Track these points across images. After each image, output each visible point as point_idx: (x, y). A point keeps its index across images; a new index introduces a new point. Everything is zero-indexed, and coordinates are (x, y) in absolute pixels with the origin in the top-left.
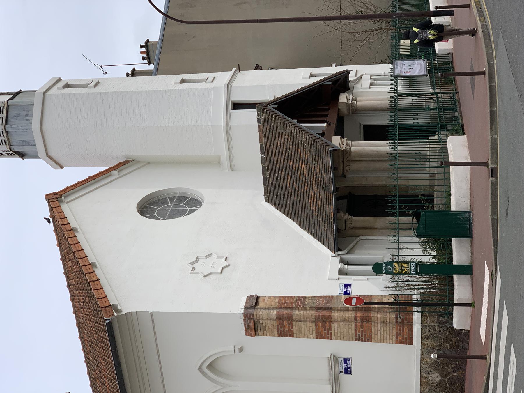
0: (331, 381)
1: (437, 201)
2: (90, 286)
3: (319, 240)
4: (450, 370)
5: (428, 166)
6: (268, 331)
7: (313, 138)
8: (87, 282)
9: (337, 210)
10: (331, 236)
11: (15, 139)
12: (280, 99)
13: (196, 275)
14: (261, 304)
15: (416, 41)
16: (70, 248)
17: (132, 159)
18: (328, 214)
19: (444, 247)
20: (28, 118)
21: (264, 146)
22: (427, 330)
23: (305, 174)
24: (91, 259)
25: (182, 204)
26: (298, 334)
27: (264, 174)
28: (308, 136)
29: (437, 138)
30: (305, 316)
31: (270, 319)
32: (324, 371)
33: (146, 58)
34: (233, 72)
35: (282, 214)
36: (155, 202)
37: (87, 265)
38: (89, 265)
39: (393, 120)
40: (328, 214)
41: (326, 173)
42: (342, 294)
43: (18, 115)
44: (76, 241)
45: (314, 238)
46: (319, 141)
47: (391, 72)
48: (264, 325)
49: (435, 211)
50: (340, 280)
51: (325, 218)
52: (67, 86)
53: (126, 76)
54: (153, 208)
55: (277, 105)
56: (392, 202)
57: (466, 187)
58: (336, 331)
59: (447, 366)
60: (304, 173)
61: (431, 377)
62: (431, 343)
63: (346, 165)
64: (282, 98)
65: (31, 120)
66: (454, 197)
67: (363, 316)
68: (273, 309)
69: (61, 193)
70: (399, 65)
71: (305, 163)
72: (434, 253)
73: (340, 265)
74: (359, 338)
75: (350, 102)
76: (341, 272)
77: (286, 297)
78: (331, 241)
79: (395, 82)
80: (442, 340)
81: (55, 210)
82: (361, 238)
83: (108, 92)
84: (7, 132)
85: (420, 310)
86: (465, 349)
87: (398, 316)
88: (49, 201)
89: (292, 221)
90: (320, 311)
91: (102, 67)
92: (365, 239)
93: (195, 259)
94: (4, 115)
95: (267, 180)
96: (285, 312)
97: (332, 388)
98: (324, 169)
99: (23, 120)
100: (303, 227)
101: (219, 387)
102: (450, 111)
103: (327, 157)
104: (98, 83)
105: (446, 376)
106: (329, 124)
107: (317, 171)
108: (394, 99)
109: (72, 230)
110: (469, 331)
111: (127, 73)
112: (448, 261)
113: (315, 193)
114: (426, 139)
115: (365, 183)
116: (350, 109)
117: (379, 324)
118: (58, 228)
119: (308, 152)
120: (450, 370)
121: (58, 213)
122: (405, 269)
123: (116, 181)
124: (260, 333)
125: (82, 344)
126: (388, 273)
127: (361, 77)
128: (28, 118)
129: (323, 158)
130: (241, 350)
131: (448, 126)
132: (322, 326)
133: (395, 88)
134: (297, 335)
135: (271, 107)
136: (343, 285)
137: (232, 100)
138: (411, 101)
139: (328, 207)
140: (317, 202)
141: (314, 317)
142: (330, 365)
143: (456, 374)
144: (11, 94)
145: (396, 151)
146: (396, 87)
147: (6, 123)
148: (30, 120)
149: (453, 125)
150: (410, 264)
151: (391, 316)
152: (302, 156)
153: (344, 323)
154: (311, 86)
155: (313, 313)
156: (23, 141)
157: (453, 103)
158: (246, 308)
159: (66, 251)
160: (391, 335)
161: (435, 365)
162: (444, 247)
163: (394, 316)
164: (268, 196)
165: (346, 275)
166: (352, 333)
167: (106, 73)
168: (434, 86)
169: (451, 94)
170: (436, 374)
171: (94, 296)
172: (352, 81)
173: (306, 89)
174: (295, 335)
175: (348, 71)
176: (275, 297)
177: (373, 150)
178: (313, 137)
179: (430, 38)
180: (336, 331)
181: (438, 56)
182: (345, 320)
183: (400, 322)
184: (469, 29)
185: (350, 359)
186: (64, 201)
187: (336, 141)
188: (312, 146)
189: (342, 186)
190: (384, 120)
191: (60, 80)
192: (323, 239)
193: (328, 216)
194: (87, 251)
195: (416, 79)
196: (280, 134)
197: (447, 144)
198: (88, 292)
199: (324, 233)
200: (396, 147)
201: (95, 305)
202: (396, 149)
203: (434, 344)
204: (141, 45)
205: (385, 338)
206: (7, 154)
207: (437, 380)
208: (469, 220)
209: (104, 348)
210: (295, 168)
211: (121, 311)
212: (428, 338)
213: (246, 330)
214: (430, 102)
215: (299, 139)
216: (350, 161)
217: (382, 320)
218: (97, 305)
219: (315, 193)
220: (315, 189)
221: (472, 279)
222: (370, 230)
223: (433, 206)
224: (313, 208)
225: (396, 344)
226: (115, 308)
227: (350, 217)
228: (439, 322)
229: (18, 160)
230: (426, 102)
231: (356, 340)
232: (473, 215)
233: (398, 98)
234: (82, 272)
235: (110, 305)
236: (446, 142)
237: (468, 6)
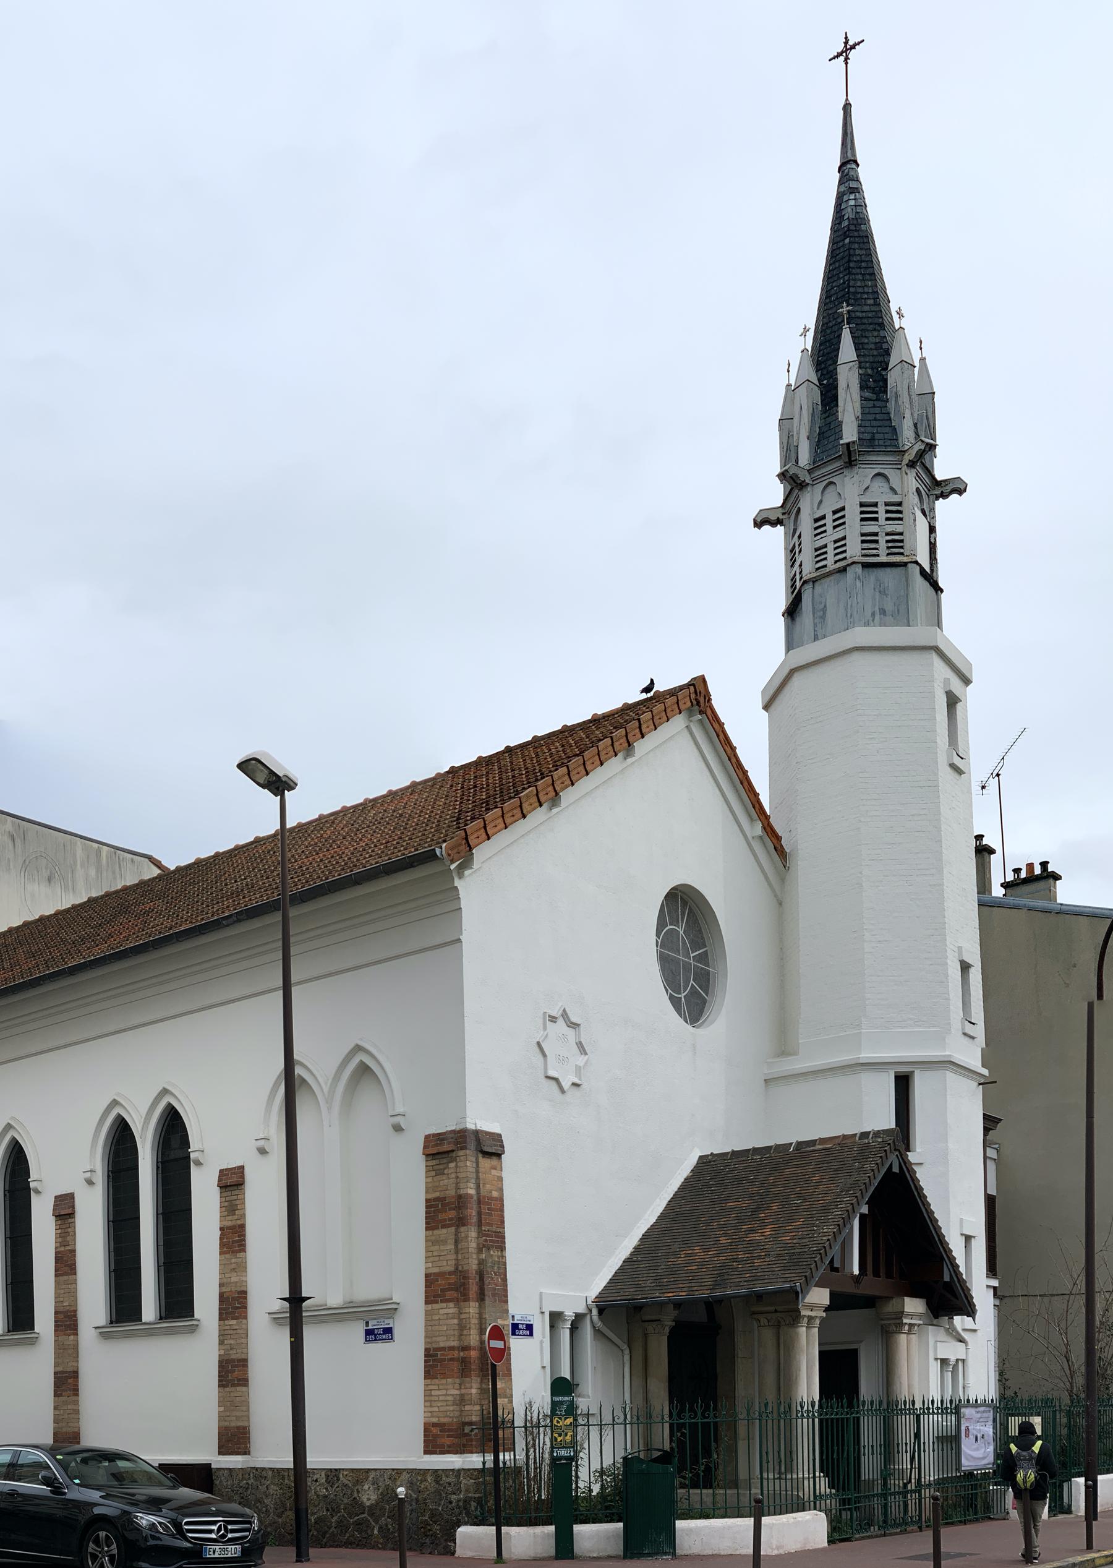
0: (350, 1304)
1: (695, 1494)
2: (511, 798)
3: (620, 1271)
4: (383, 1521)
5: (765, 1475)
6: (435, 1179)
7: (824, 1250)
8: (517, 791)
9: (678, 1305)
10: (627, 1294)
11: (829, 591)
12: (911, 1177)
13: (542, 1026)
14: (485, 1163)
15: (1013, 1448)
16: (591, 745)
17: (788, 865)
18: (669, 1287)
19: (607, 1508)
20: (877, 617)
21: (812, 1148)
22: (452, 1479)
23: (751, 1237)
24: (568, 796)
25: (692, 982)
26: (433, 1238)
27: (755, 1151)
28: (828, 1240)
29: (823, 1492)
30: (466, 1251)
31: (457, 1183)
32: (367, 1291)
33: (1018, 876)
34: (979, 1071)
35: (674, 1193)
36: (696, 922)
37: (554, 788)
38: (555, 791)
39: (872, 1407)
40: (669, 1287)
41: (751, 1279)
42: (513, 1320)
43: (883, 593)
44: (607, 756)
45: (623, 1260)
46: (815, 1262)
47: (968, 1401)
48: (446, 1172)
49: (673, 1490)
50: (540, 1315)
51: (662, 1281)
52: (952, 701)
53: (976, 834)
54: (682, 921)
55: (898, 1171)
56: (692, 1410)
57: (724, 1547)
58: (442, 1312)
59: (388, 1517)
60: (754, 1235)
61: (369, 1488)
62: (429, 1487)
63: (769, 1318)
64: (913, 1180)
65: (872, 624)
66: (702, 1525)
67: (472, 1361)
68: (478, 1188)
69: (709, 712)
70: (985, 1415)
71: (774, 1236)
72: (596, 1489)
73: (570, 1314)
74: (431, 1356)
75: (905, 1321)
76: (555, 1318)
77: (502, 1210)
78: (616, 1295)
79: (947, 1408)
80: (434, 1507)
81: (671, 701)
82: (627, 1352)
83: (939, 797)
84: (843, 570)
85: (487, 1466)
86: (421, 1548)
87: (474, 1427)
88: (691, 685)
89: (659, 1214)
90: (477, 1280)
91: (997, 778)
92: (625, 1360)
93: (574, 1019)
94: (883, 559)
95: (742, 1159)
96: (472, 1212)
97: (337, 1306)
98: (759, 1274)
99: (874, 606)
100: (646, 1237)
101: (326, 1090)
102: (880, 1516)
103: (783, 1280)
104: (959, 771)
105: (372, 1515)
106: (857, 1280)
107: (756, 1261)
108: (910, 1408)
109: (629, 745)
110: (453, 1553)
111: (983, 836)
112: (581, 1515)
113: (713, 1259)
114: (821, 1471)
115: (740, 1356)
116: (889, 1322)
117: (457, 1392)
118: (631, 713)
119: (795, 1241)
120: (384, 1522)
121: (665, 711)
122: (561, 1438)
123: (739, 831)
124: (430, 1163)
125: (401, 790)
126: (554, 1405)
127: (961, 1340)
128: (877, 617)
129: (782, 1272)
130: (398, 1128)
131: (849, 1513)
132: (449, 1284)
133: (933, 1409)
134: (429, 1238)
135: (893, 1158)
136: (530, 1321)
137: (916, 1073)
138: (904, 1441)
139: (684, 1285)
140: (694, 1264)
141: (465, 1269)
142: (379, 1302)
143: (376, 1532)
144: (932, 571)
145: (797, 1416)
146: (936, 1411)
147: (865, 566)
148: (873, 621)
149: (852, 1522)
150: (572, 1447)
151: (474, 1413)
152: (787, 1228)
153: (457, 1327)
154: (940, 1240)
155: (473, 1265)
156: (824, 610)
157: (898, 1521)
158: (477, 1133)
159: (584, 736)
160: (440, 1414)
161: (389, 1494)
162: (607, 1508)
163: (474, 1420)
164: (710, 1162)
165: (550, 1327)
166: (438, 1342)
167: (983, 787)
168: (935, 1485)
169: (917, 1518)
170: (374, 1497)
171: (488, 810)
172: (953, 1323)
173: (935, 1229)
174: (430, 1232)
175: (973, 1313)
176: (501, 1190)
177: (800, 1370)
178: (825, 1251)
179: (1019, 1475)
180: (442, 1312)
181: (1003, 1493)
182: (462, 1327)
183: (464, 1430)
184: (1037, 1549)
185: (392, 1339)
186: (691, 721)
187: (820, 1296)
188: (806, 1250)
189: (734, 1310)
190: (868, 1388)
191: (967, 681)
192: (622, 1277)
193: (666, 1287)
194: (585, 785)
195: (952, 1449)
196: (835, 1182)
197: (810, 1510)
198: (498, 796)
199: (633, 1280)
200: (805, 1415)
201: (469, 814)
202: (799, 1415)
203: (428, 1493)
204: (1048, 862)
205: (434, 1404)
206: (795, 575)
207: (364, 1498)
208: (657, 1554)
209: (389, 845)
210: (763, 1215)
211: (461, 876)
212: (437, 1482)
213: (434, 1135)
214: (901, 1477)
215: (822, 1221)
216: (778, 1326)
217: (467, 1398)
218: (471, 819)
219: (713, 1259)
220: (721, 1258)
221: (549, 1558)
222: (642, 1369)
223: (683, 1486)
224: (682, 1256)
225: (425, 1423)
226: (467, 863)
227: (667, 1330)
228: (467, 1501)
229: (781, 602)
230: (901, 1471)
231: (426, 1350)
232: (667, 1559)
233: (912, 1416)
234: (539, 778)
235: (471, 849)
236: (815, 1509)
237: (1089, 1546)
